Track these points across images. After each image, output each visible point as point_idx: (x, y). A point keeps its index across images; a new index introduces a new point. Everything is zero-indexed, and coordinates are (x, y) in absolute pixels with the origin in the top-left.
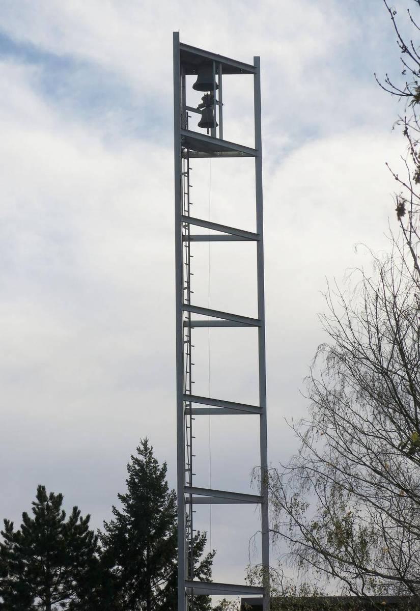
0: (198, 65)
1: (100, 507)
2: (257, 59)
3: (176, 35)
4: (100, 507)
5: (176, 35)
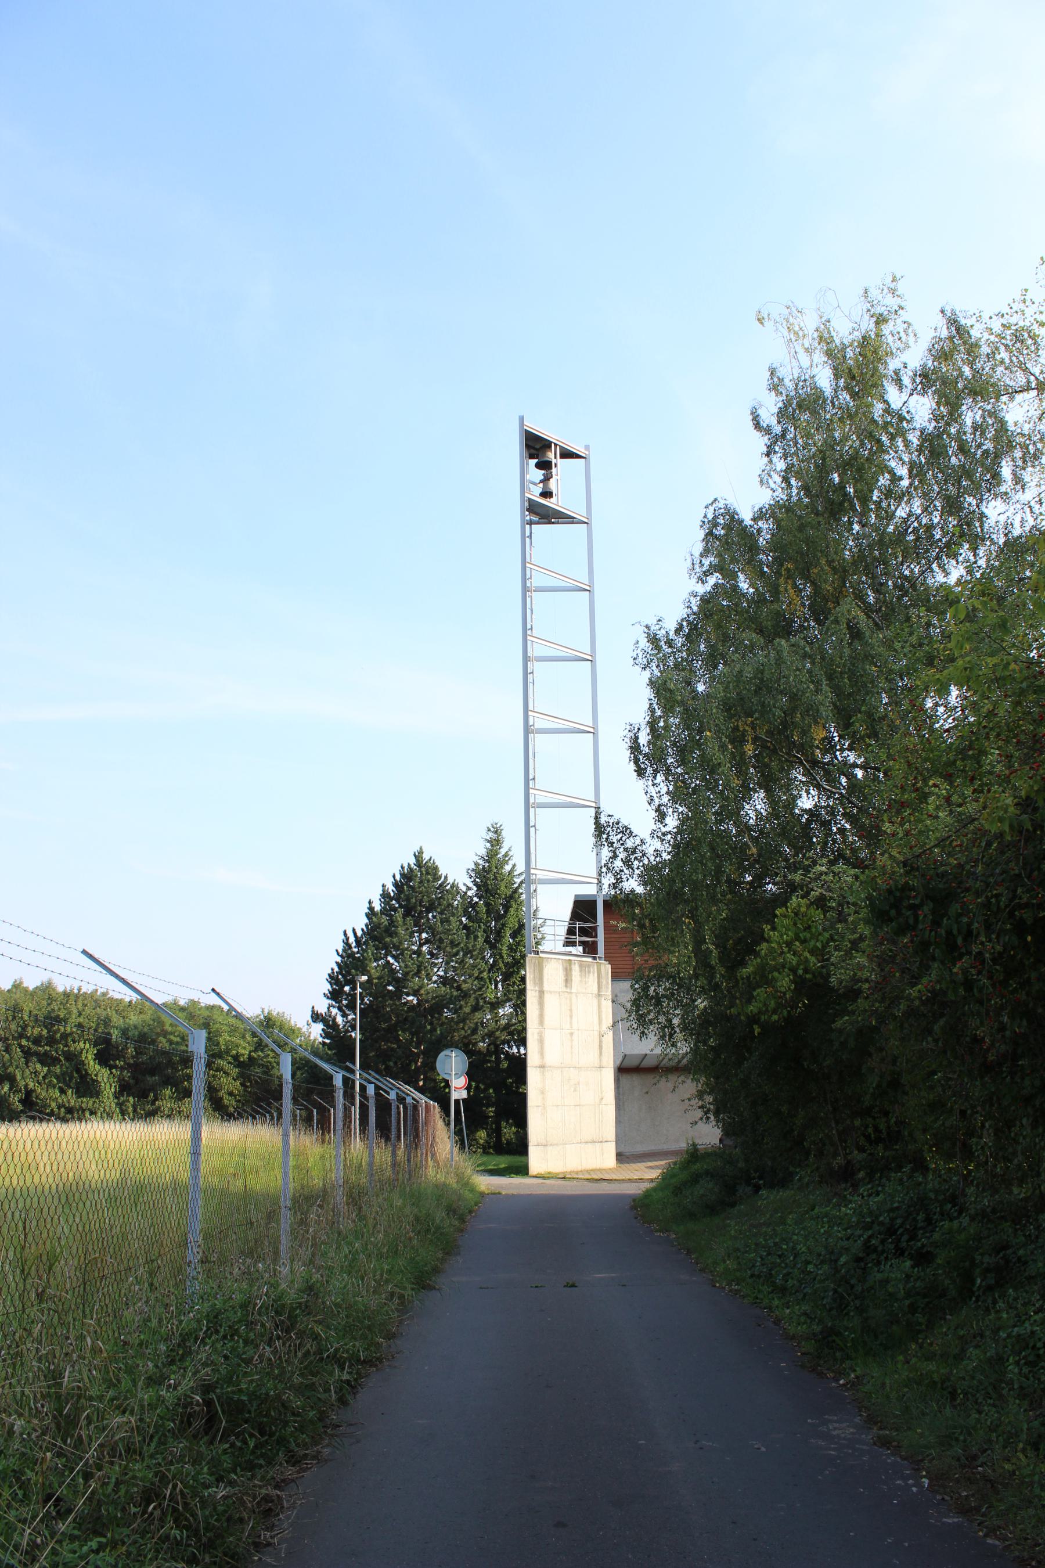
0: (536, 447)
1: (457, 870)
2: (587, 447)
3: (522, 419)
4: (457, 870)
5: (522, 419)
